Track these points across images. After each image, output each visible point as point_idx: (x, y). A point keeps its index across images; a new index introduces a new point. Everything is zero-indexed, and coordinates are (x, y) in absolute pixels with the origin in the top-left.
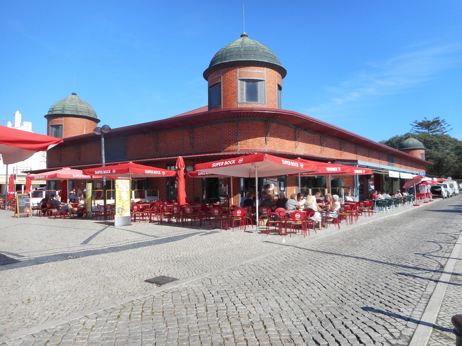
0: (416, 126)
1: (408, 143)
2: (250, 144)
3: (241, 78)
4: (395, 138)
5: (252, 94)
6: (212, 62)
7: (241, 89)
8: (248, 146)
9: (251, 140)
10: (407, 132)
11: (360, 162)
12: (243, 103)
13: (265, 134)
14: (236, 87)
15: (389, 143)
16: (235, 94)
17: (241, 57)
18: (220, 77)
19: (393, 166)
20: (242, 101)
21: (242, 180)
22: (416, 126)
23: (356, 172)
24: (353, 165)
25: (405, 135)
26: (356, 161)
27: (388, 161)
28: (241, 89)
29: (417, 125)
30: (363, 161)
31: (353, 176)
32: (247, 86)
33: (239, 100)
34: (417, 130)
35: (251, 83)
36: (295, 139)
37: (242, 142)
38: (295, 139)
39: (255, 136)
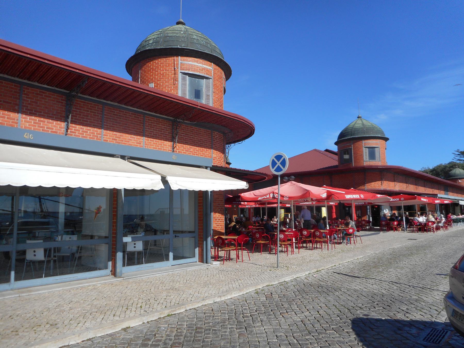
0: (458, 155)
1: (455, 174)
2: (373, 186)
3: (183, 71)
4: (439, 166)
5: (372, 155)
6: (137, 51)
7: (366, 152)
8: (371, 187)
9: (373, 183)
10: (451, 160)
11: (439, 196)
12: (366, 161)
13: (381, 179)
14: (363, 152)
15: (435, 171)
16: (362, 156)
17: (365, 134)
18: (351, 145)
19: (448, 195)
20: (367, 162)
21: (334, 207)
22: (458, 155)
23: (437, 202)
24: (434, 197)
25: (449, 164)
26: (437, 195)
27: (444, 191)
28: (366, 152)
29: (459, 153)
30: (441, 195)
31: (435, 205)
32: (191, 83)
33: (365, 159)
34: (459, 158)
35: (371, 149)
36: (394, 181)
37: (368, 184)
38: (394, 181)
39: (375, 181)
